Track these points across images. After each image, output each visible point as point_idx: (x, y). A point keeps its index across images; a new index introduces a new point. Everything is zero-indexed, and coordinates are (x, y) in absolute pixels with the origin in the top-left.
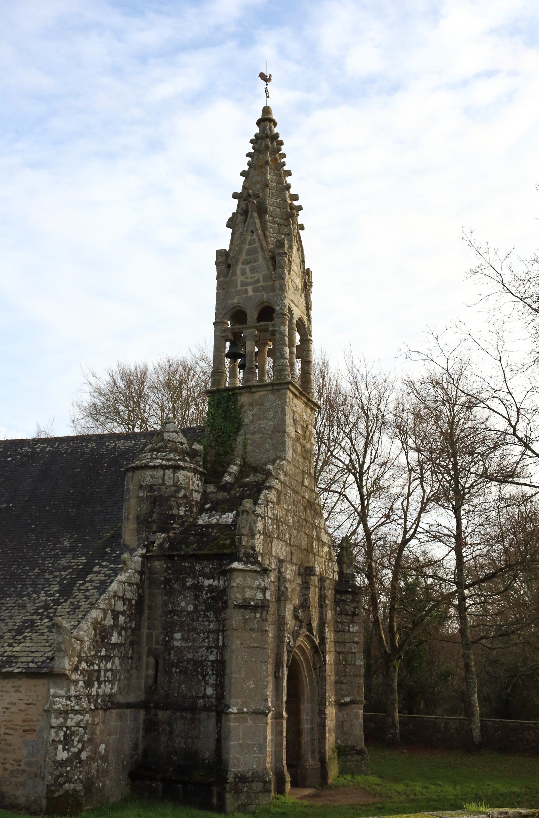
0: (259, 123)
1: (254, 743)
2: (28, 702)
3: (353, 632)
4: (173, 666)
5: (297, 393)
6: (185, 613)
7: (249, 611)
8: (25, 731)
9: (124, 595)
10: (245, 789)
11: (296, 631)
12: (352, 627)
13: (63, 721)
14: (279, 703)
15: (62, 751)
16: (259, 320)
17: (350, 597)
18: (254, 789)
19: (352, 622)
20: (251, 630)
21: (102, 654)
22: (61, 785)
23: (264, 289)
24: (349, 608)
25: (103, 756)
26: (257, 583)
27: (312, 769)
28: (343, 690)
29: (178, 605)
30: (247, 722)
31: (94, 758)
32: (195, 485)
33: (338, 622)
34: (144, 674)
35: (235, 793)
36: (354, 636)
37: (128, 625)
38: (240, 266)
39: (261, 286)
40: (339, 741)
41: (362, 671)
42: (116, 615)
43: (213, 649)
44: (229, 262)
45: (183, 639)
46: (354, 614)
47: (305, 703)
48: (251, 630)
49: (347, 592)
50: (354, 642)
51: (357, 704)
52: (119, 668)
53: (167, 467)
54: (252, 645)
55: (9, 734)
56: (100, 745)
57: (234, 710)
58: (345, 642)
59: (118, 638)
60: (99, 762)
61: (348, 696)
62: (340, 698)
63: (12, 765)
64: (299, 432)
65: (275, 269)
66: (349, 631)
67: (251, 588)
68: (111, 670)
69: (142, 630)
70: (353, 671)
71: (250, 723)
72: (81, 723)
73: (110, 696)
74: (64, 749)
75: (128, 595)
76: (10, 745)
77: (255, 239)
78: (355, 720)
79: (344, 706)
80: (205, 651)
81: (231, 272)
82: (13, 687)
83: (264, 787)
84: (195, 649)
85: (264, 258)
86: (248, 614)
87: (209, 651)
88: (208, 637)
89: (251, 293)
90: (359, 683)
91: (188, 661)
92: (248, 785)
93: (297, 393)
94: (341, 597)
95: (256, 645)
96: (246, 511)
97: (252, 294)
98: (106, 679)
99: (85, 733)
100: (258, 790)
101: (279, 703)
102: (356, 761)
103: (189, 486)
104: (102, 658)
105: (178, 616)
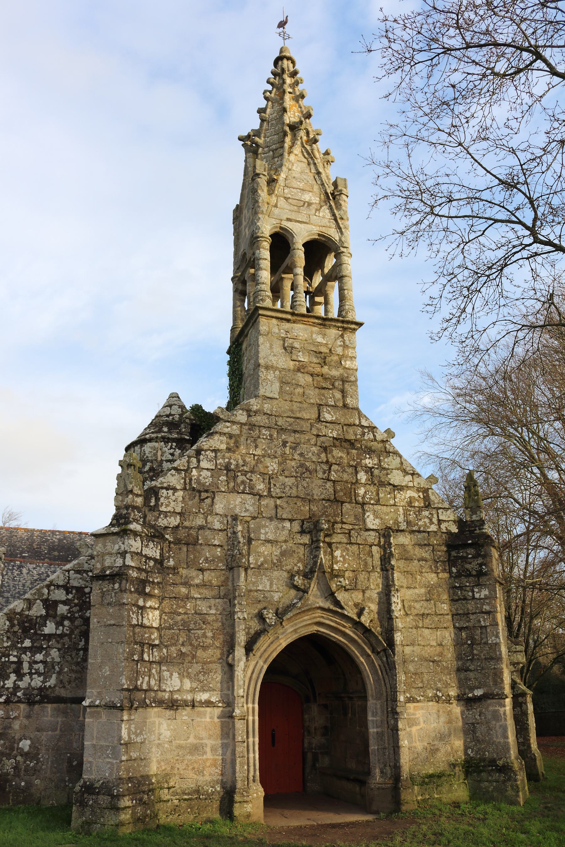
1: (107, 744)
3: (480, 599)
5: (289, 317)
7: (107, 582)
9: (68, 583)
10: (91, 802)
12: (479, 592)
17: (471, 551)
18: (100, 804)
19: (478, 585)
20: (108, 604)
24: (472, 566)
26: (117, 547)
27: (379, 788)
28: (470, 680)
30: (101, 717)
33: (456, 587)
35: (80, 806)
40: (469, 752)
46: (480, 574)
47: (370, 698)
48: (108, 604)
49: (466, 546)
50: (483, 612)
51: (493, 698)
52: (58, 660)
54: (109, 622)
58: (469, 613)
59: (57, 629)
61: (480, 688)
62: (467, 691)
66: (473, 598)
67: (110, 554)
70: (485, 652)
71: (104, 718)
75: (75, 583)
78: (494, 722)
79: (475, 702)
83: (110, 803)
86: (106, 586)
90: (495, 668)
92: (94, 797)
93: (289, 317)
94: (458, 553)
95: (112, 622)
100: (104, 806)
102: (497, 781)
103: (157, 457)
104: (25, 650)
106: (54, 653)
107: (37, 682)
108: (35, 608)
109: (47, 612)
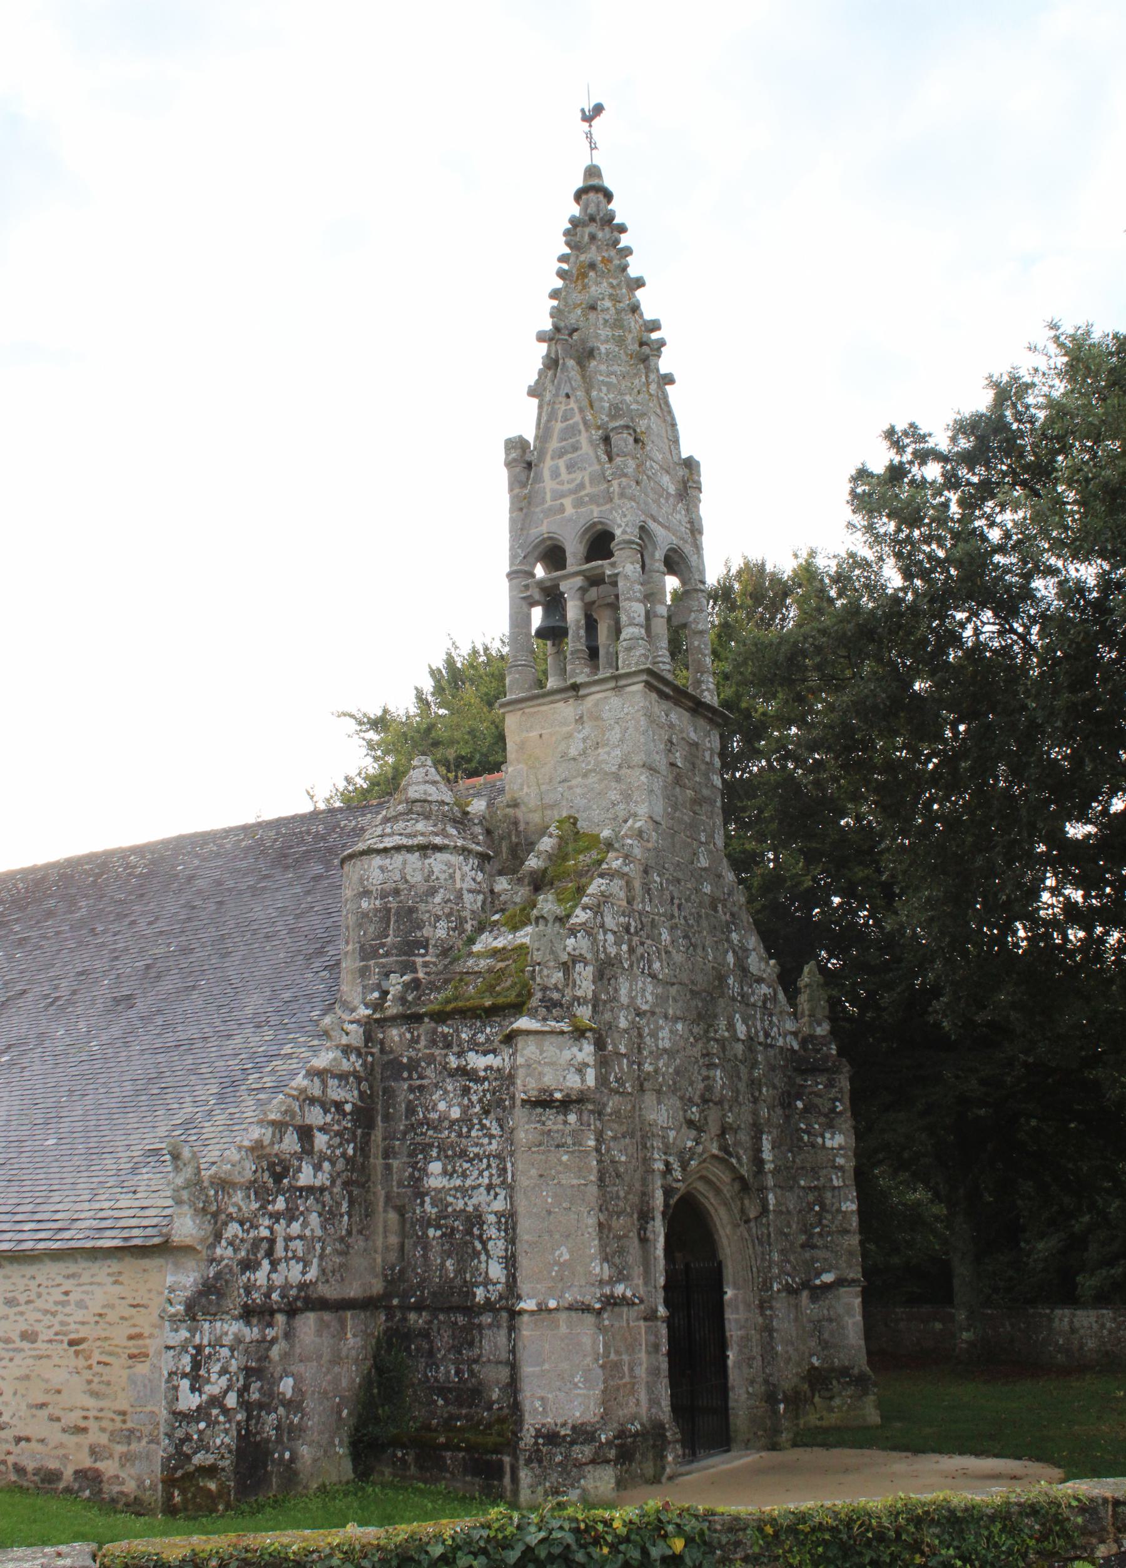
0: (579, 196)
2: (135, 1303)
3: (833, 1149)
4: (429, 1225)
6: (446, 1124)
8: (131, 1356)
11: (690, 1148)
12: (832, 1138)
13: (188, 1335)
14: (650, 1289)
15: (189, 1392)
16: (589, 559)
21: (276, 1207)
22: (188, 1458)
23: (594, 499)
25: (290, 1401)
29: (433, 1108)
31: (269, 1405)
32: (468, 879)
34: (379, 1242)
36: (835, 1156)
37: (338, 1152)
38: (548, 463)
39: (587, 495)
41: (855, 1222)
42: (305, 1134)
43: (498, 1190)
44: (528, 458)
45: (445, 1172)
52: (319, 1232)
53: (409, 849)
55: (106, 1364)
56: (281, 1378)
57: (529, 1304)
59: (315, 1177)
60: (281, 1411)
61: (829, 1272)
63: (113, 1420)
64: (679, 764)
65: (611, 459)
68: (300, 1237)
69: (372, 1160)
72: (224, 1337)
73: (302, 1286)
74: (193, 1389)
76: (108, 1384)
77: (572, 409)
78: (846, 1318)
80: (485, 1192)
81: (532, 475)
82: (109, 1274)
84: (467, 1191)
85: (591, 441)
86: (552, 1120)
87: (492, 1193)
88: (489, 1166)
89: (570, 510)
91: (457, 1214)
96: (543, 917)
97: (574, 511)
98: (290, 1254)
99: (232, 1356)
101: (650, 1289)
104: (276, 1217)
105: (435, 1129)
106: (314, 1219)
107: (293, 1273)
108: (287, 1139)
109: (302, 1147)
